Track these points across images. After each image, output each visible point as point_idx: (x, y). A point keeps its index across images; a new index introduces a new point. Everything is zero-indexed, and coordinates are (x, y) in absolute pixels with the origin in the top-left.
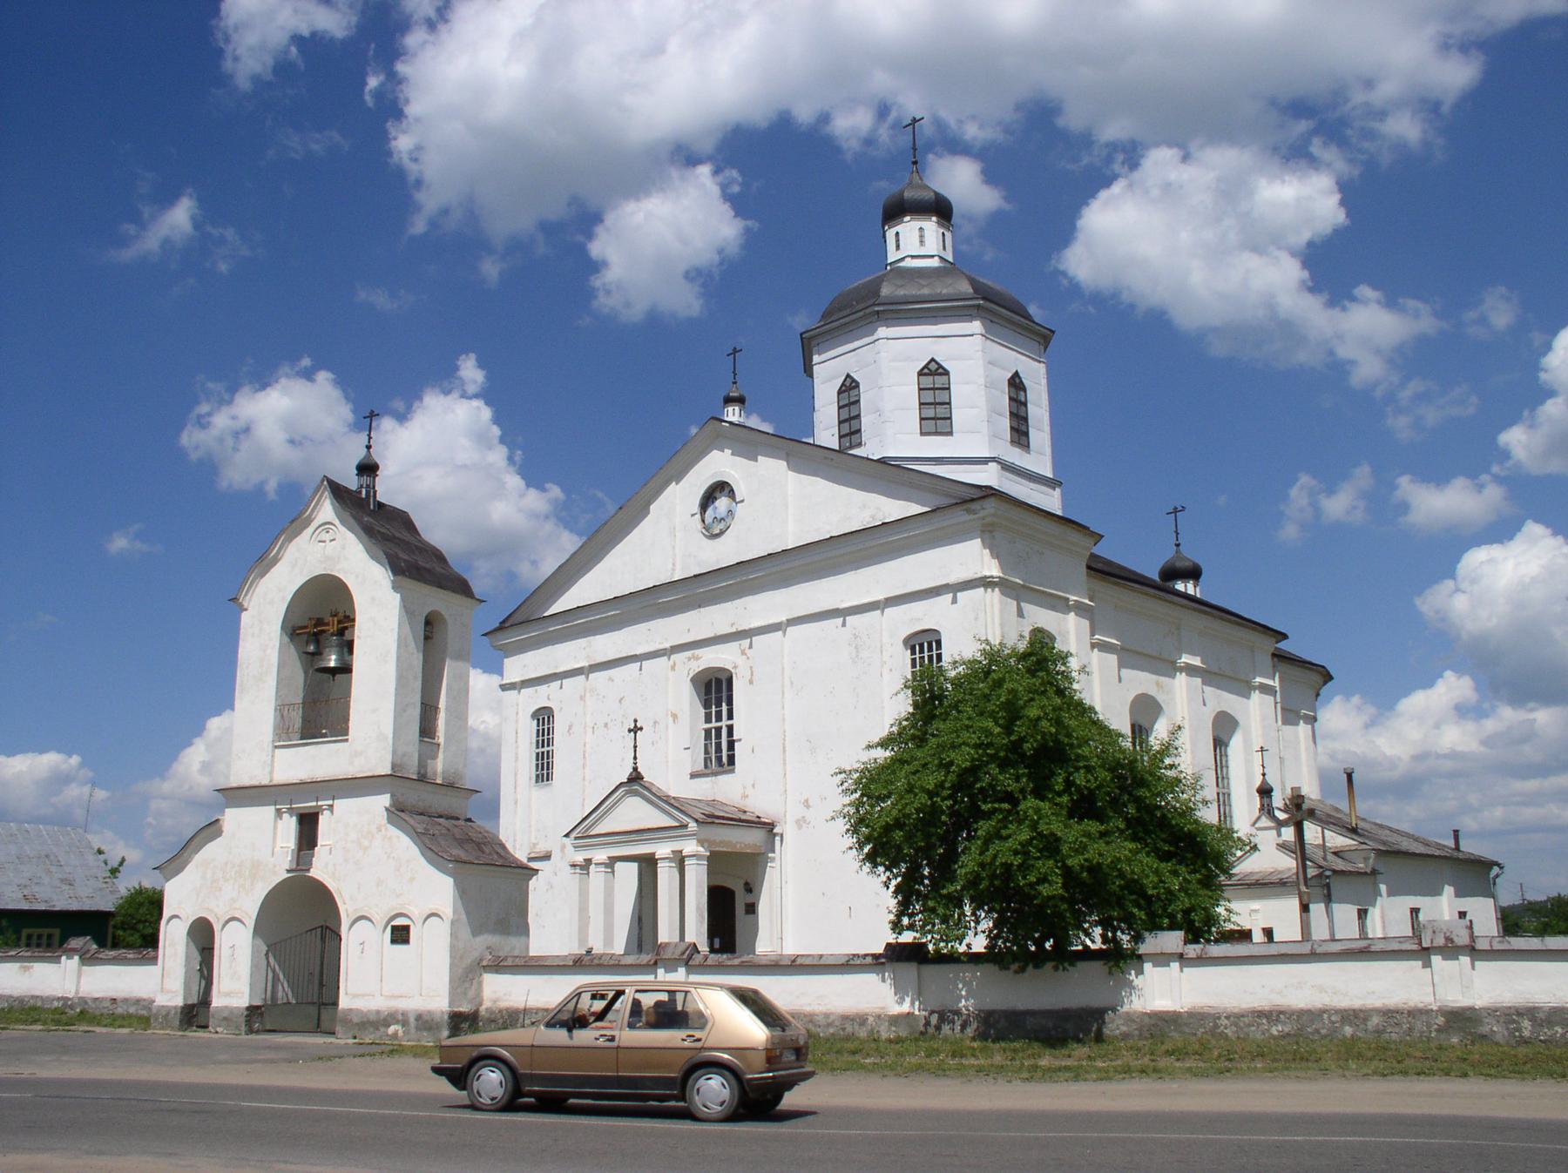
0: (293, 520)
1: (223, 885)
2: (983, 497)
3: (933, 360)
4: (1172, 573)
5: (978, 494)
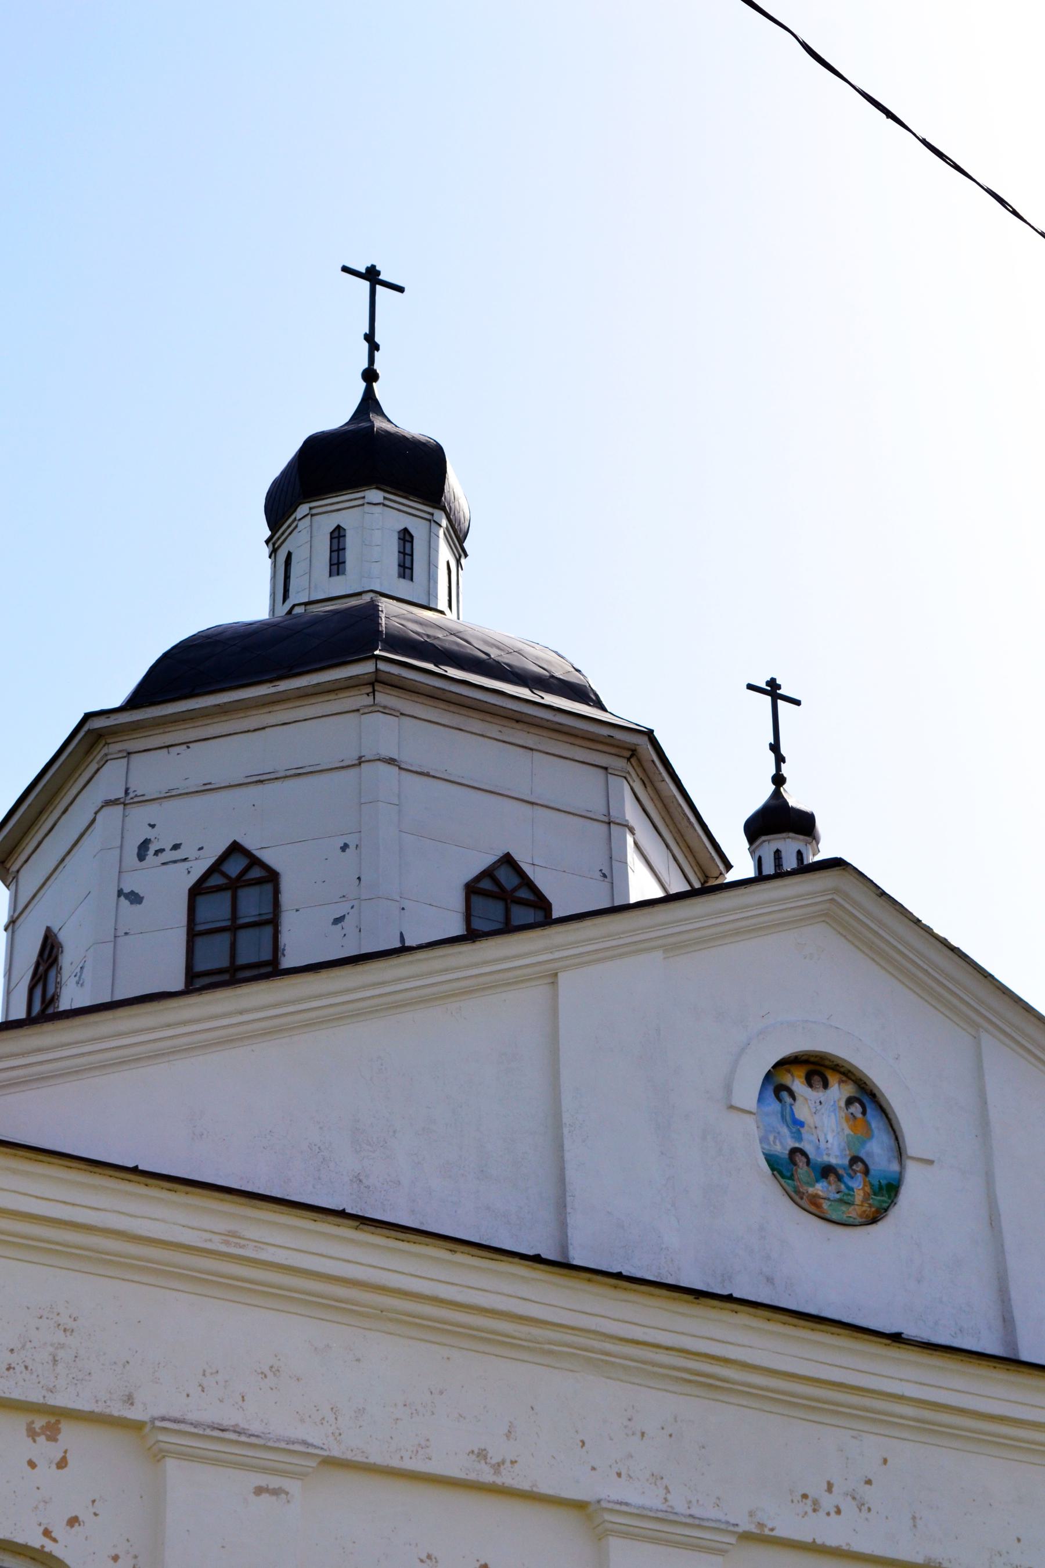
3: (235, 848)
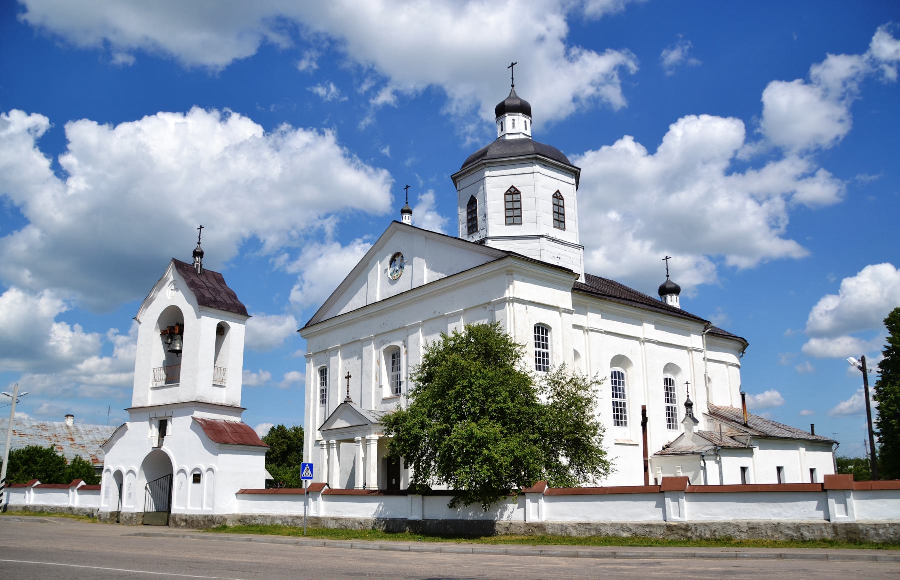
0: (159, 282)
1: (127, 455)
2: (506, 257)
4: (665, 291)
5: (505, 255)
